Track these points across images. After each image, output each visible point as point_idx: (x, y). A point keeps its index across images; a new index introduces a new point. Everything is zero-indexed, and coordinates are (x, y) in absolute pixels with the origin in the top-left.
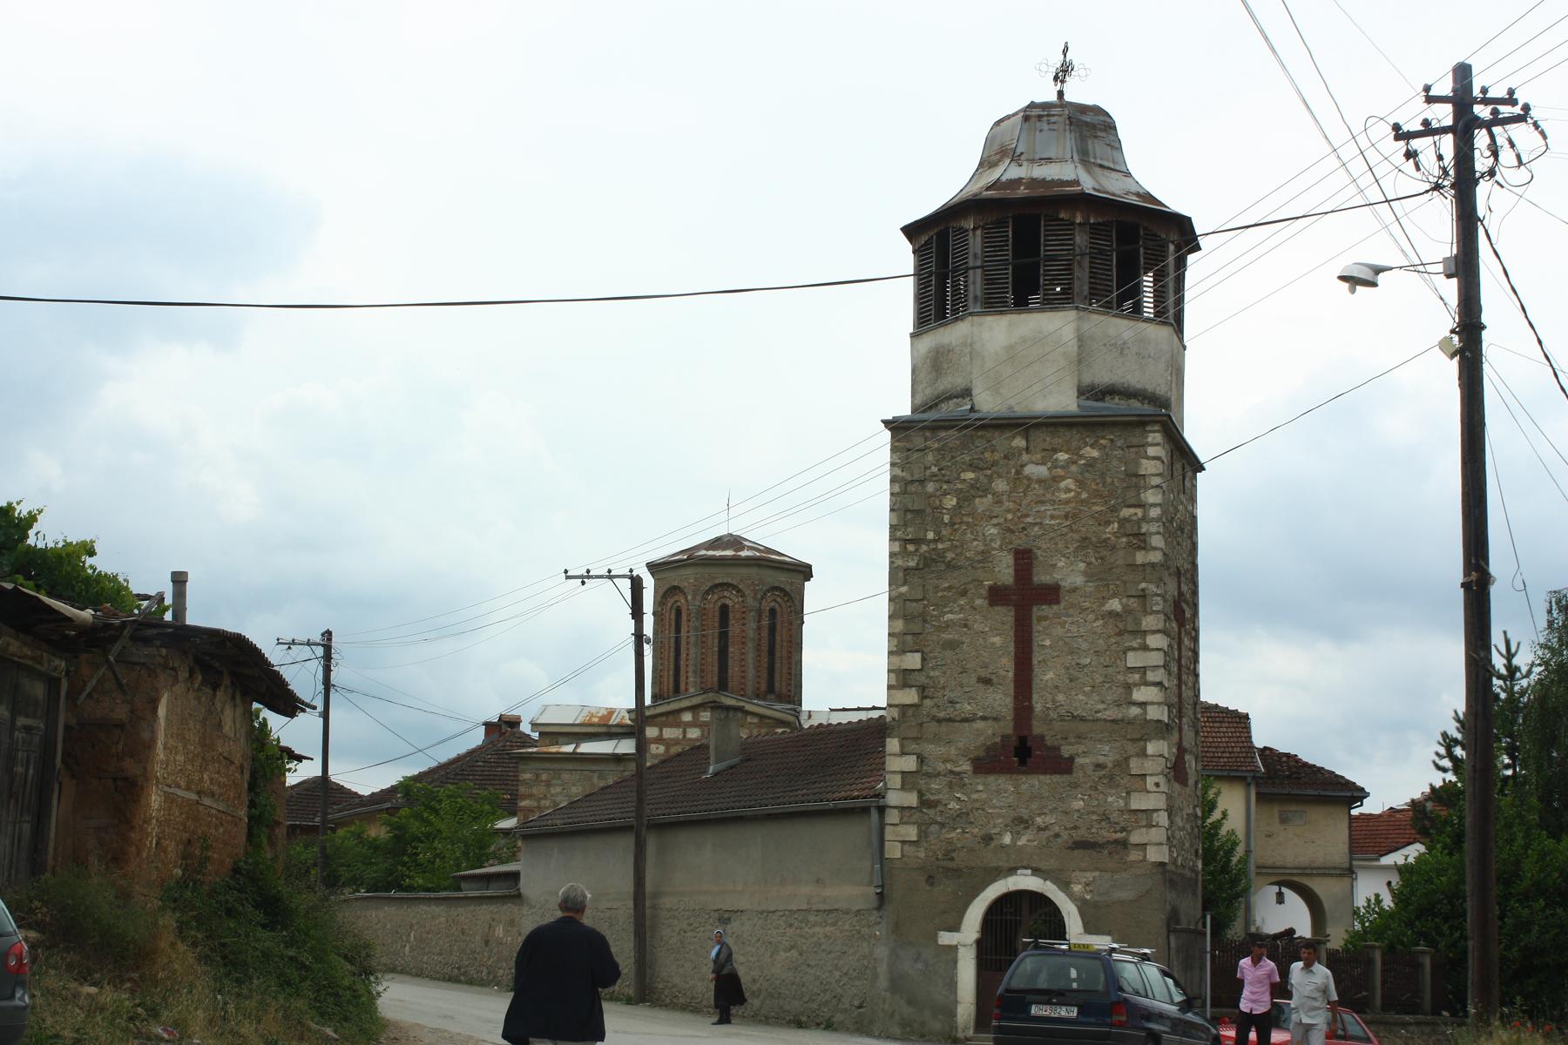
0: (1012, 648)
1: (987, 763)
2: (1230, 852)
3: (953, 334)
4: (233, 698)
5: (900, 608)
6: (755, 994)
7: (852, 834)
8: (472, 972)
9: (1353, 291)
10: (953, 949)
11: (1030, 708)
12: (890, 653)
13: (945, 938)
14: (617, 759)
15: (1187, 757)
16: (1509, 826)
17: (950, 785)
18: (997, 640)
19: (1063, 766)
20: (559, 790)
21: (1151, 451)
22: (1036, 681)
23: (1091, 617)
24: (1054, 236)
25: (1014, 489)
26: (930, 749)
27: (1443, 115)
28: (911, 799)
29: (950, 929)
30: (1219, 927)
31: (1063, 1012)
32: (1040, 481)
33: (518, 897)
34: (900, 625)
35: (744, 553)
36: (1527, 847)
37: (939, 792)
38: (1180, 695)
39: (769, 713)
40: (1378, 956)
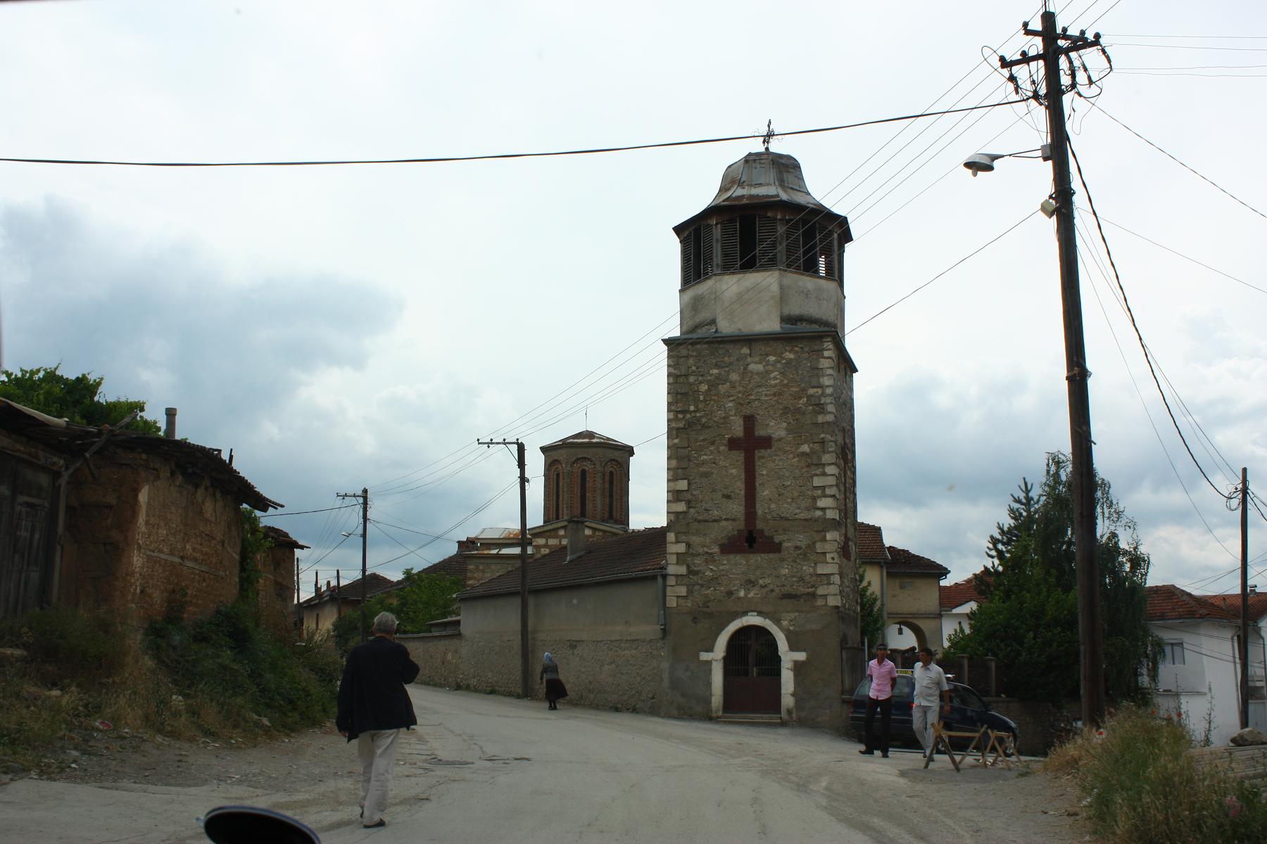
3: (704, 287)
4: (214, 495)
9: (975, 175)
10: (709, 663)
11: (755, 513)
13: (704, 656)
16: (1038, 585)
17: (706, 561)
18: (734, 471)
19: (775, 548)
21: (826, 354)
22: (758, 495)
24: (765, 231)
25: (742, 379)
26: (696, 540)
27: (1036, 45)
28: (683, 570)
29: (708, 651)
32: (758, 374)
34: (674, 463)
36: (1048, 596)
40: (966, 662)
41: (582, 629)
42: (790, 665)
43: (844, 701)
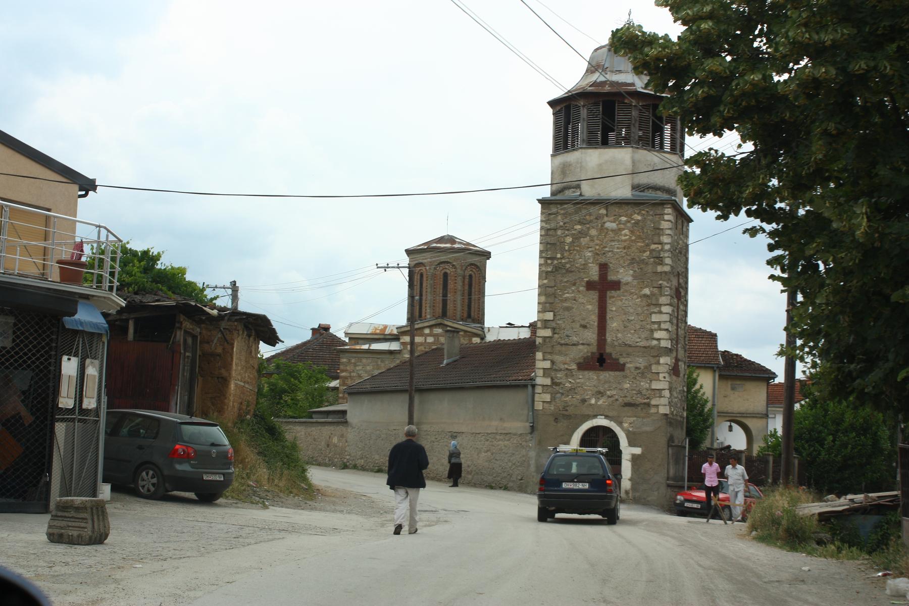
0: (597, 311)
1: (584, 365)
2: (703, 406)
3: (572, 157)
5: (544, 290)
6: (469, 473)
7: (519, 397)
8: (320, 459)
11: (605, 340)
12: (539, 312)
14: (391, 352)
15: (680, 363)
17: (566, 375)
18: (590, 307)
19: (620, 368)
20: (360, 368)
21: (666, 217)
22: (608, 327)
23: (635, 297)
26: (558, 358)
28: (548, 381)
30: (695, 444)
31: (580, 486)
32: (612, 231)
33: (346, 423)
34: (543, 299)
35: (456, 246)
37: (561, 378)
38: (677, 334)
39: (469, 329)
40: (771, 459)
41: (449, 422)
42: (629, 457)
43: (668, 486)
